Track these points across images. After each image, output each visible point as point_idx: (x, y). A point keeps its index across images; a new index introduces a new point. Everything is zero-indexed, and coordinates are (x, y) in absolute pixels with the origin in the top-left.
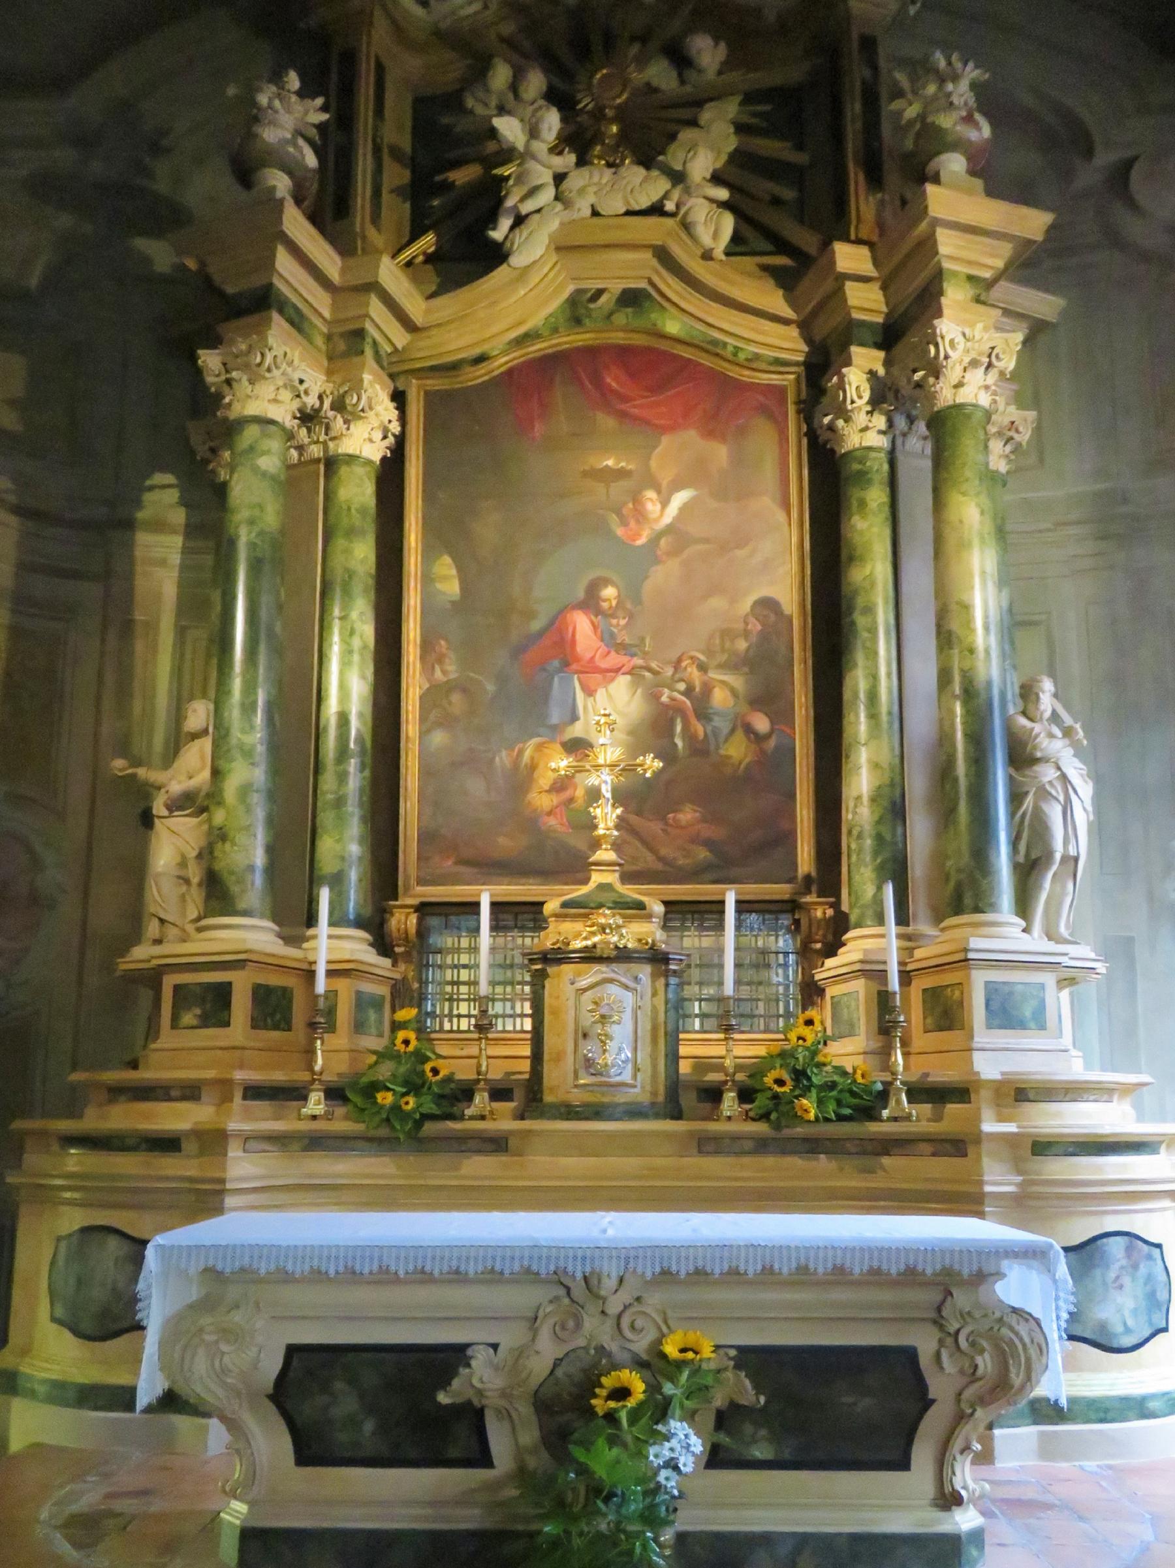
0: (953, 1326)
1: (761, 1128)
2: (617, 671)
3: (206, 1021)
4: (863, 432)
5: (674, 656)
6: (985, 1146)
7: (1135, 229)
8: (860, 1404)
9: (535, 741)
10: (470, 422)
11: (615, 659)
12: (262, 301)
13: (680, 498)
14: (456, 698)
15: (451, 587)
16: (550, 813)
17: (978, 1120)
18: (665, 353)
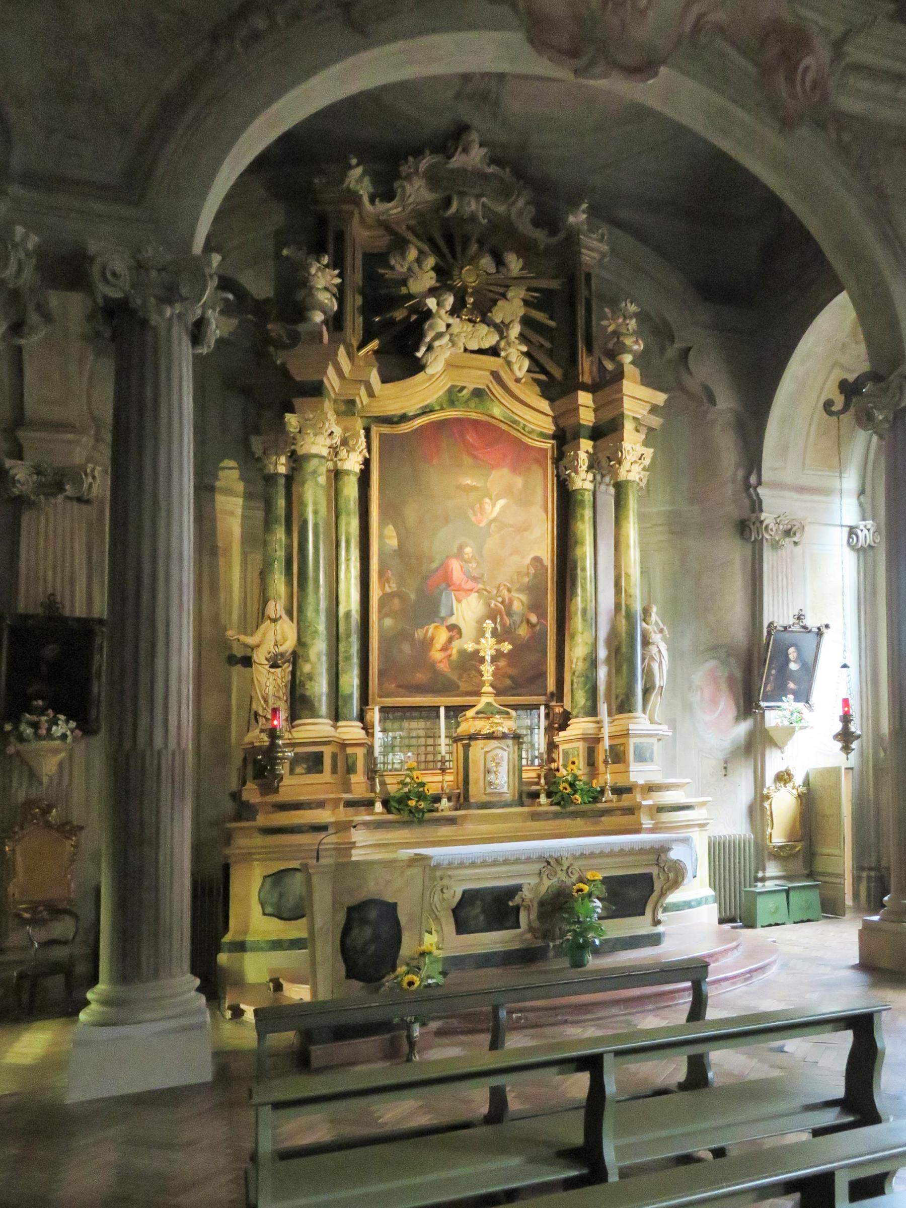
0: (662, 865)
2: (471, 590)
3: (309, 771)
4: (583, 481)
5: (498, 583)
6: (642, 810)
7: (687, 381)
8: (632, 893)
9: (433, 625)
10: (404, 447)
11: (470, 585)
12: (316, 390)
14: (396, 601)
15: (393, 543)
16: (441, 662)
18: (494, 426)
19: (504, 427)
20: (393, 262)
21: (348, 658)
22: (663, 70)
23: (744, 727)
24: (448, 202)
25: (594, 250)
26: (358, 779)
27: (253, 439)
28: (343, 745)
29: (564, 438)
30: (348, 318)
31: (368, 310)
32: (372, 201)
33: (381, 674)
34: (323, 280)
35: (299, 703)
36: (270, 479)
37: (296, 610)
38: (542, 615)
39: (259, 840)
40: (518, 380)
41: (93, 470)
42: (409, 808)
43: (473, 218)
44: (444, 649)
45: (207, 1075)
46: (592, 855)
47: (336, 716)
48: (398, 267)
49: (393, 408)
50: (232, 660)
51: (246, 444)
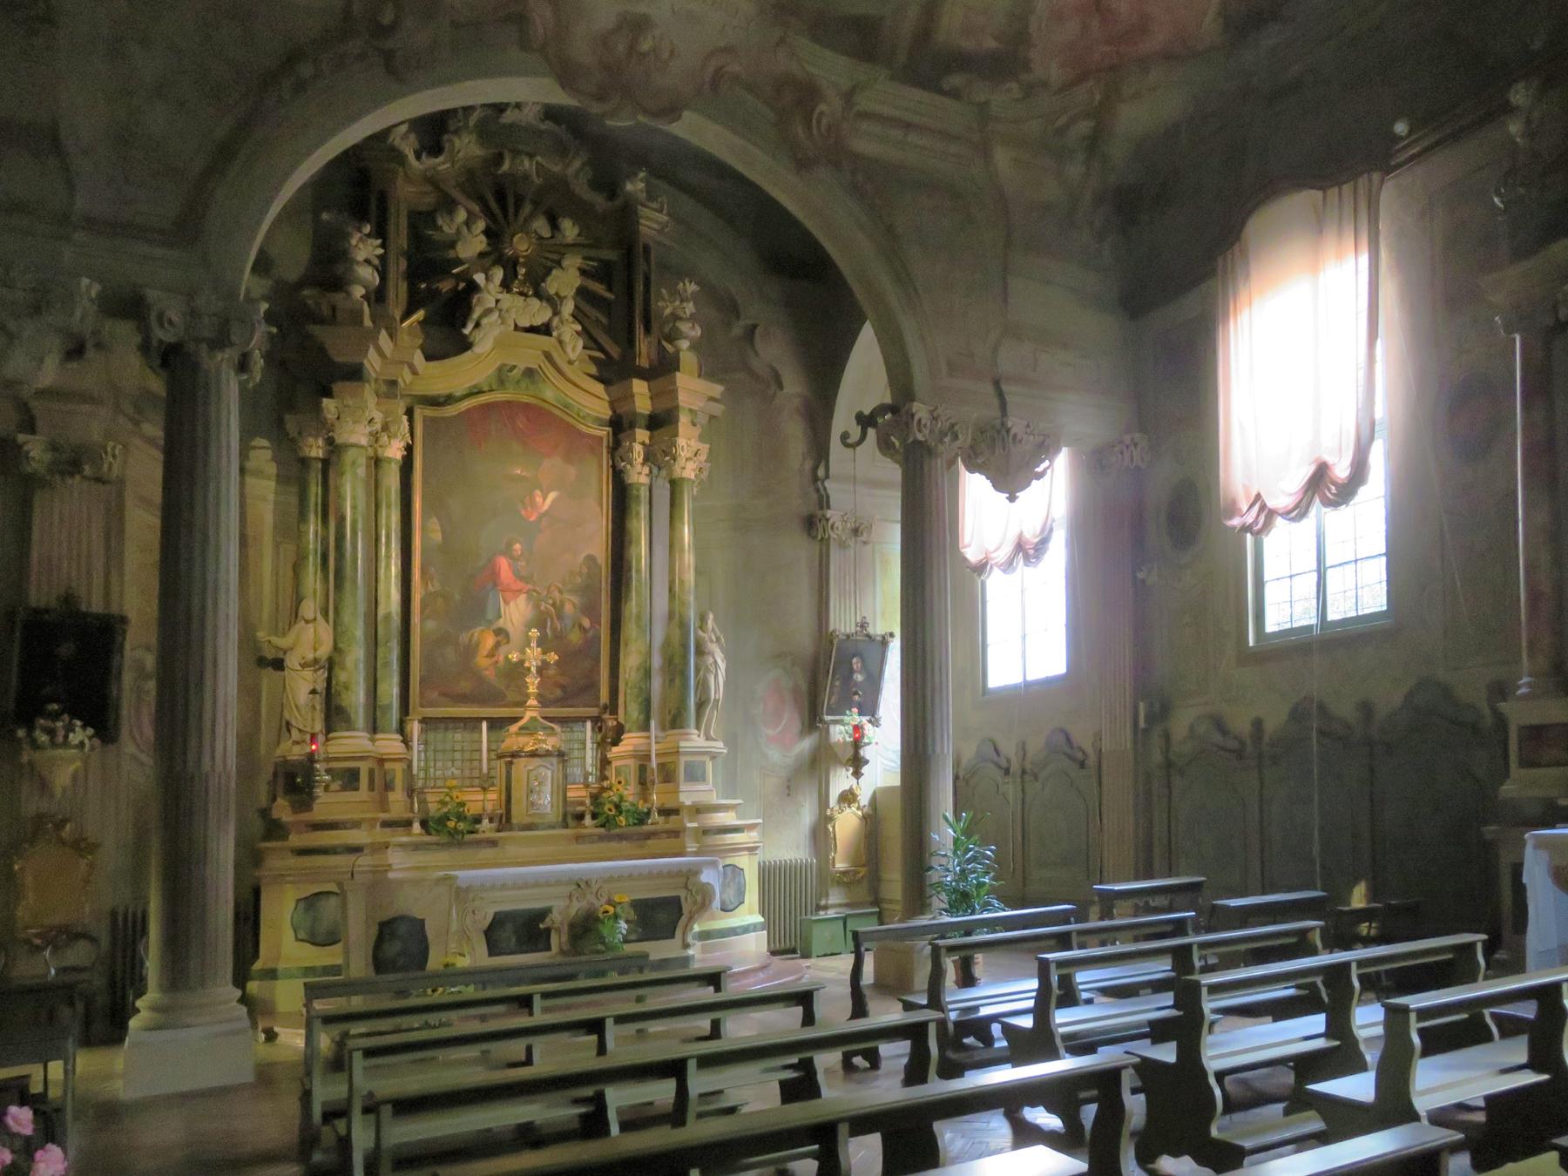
1: (602, 830)
2: (520, 591)
3: (344, 788)
4: (638, 474)
8: (662, 917)
11: (521, 585)
12: (355, 374)
13: (552, 496)
14: (440, 601)
15: (437, 537)
17: (682, 821)
19: (558, 412)
20: (440, 222)
21: (387, 664)
22: (686, 114)
23: (806, 744)
24: (498, 159)
25: (652, 222)
26: (397, 797)
27: (287, 417)
28: (381, 761)
29: (620, 425)
30: (391, 294)
31: (413, 276)
32: (418, 157)
33: (422, 680)
34: (364, 249)
35: (334, 715)
36: (304, 462)
37: (332, 611)
38: (596, 621)
39: (293, 861)
40: (570, 362)
41: (114, 448)
42: (449, 829)
43: (526, 177)
44: (491, 654)
45: (249, 1077)
46: (620, 878)
47: (374, 728)
48: (446, 229)
49: (438, 388)
50: (262, 662)
51: (280, 423)
